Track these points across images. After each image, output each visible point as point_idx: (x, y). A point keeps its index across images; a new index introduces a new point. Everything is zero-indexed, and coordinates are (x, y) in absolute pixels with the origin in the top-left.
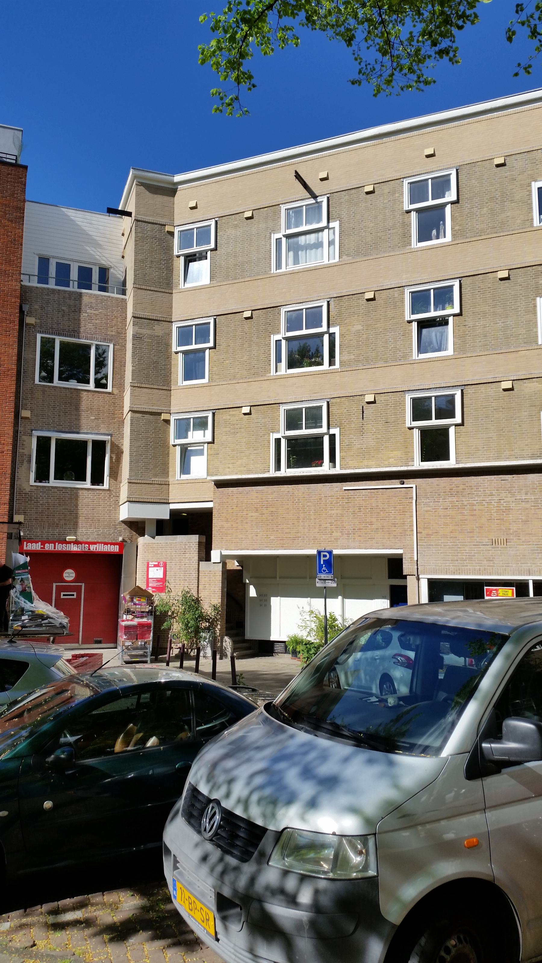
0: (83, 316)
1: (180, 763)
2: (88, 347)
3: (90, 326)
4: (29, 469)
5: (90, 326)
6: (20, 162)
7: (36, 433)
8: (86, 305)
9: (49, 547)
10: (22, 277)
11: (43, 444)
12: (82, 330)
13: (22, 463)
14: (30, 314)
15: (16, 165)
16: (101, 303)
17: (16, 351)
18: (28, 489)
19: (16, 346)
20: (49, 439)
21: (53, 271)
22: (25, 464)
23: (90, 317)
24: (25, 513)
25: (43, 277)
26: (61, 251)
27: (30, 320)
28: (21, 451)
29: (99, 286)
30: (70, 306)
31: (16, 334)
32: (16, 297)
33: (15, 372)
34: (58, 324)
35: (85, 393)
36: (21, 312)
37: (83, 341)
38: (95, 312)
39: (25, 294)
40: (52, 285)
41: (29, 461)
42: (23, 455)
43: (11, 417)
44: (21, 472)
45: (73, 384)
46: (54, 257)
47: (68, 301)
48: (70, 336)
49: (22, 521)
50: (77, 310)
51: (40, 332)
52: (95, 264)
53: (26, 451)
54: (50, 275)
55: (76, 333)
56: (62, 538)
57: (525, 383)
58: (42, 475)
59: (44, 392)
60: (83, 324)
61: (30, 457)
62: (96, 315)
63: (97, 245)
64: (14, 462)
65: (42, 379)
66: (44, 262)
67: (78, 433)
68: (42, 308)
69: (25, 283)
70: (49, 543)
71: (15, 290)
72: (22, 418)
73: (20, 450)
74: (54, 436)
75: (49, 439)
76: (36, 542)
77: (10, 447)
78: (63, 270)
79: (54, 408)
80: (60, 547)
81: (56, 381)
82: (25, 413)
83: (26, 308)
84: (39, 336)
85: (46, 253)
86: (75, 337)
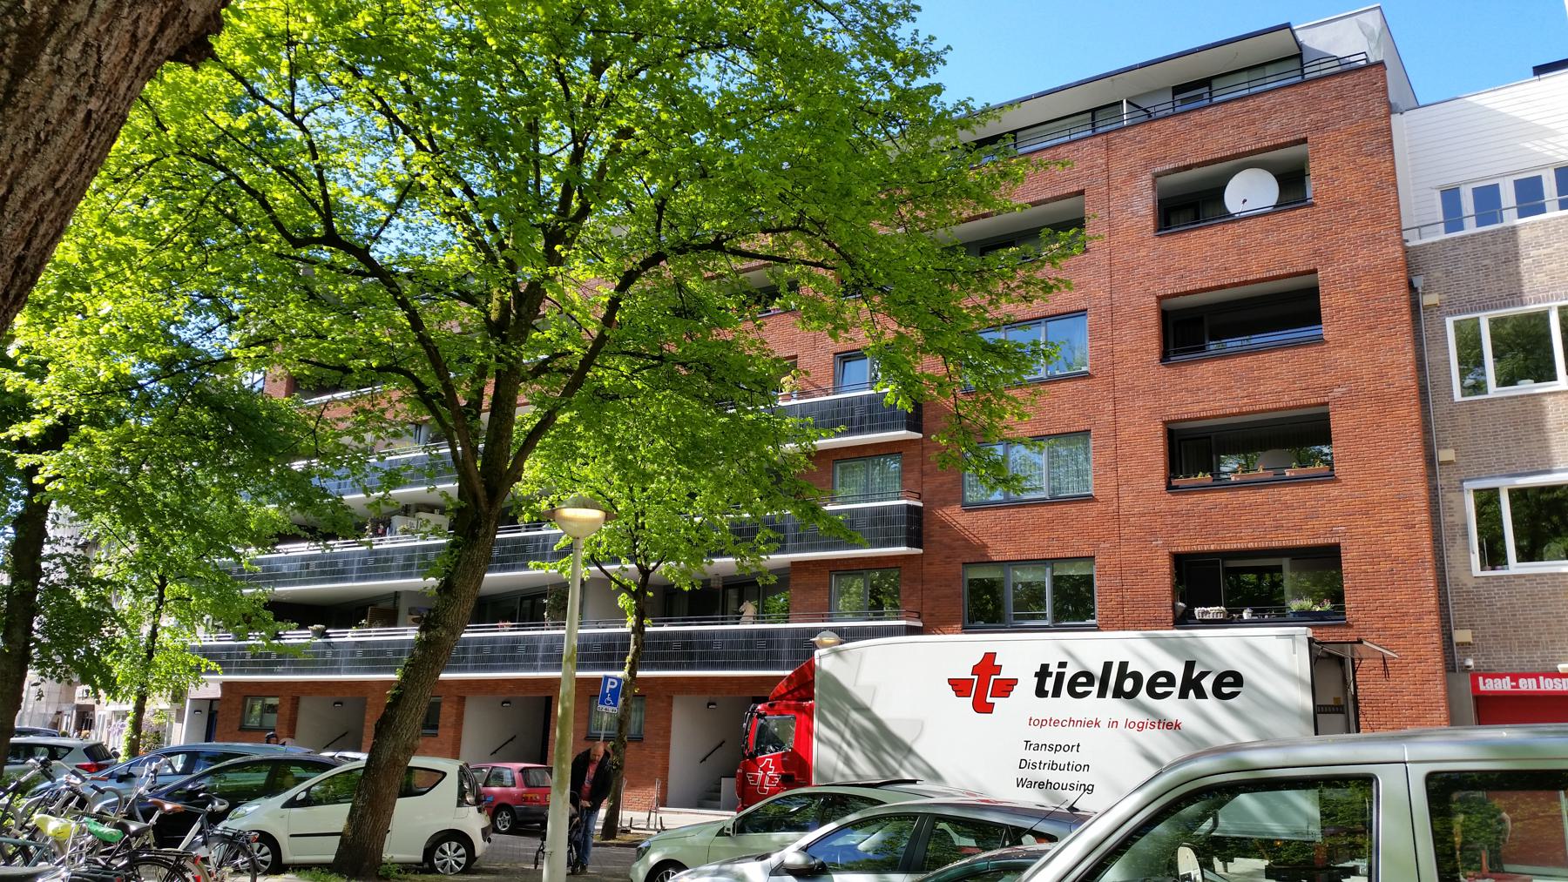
0: (1525, 264)
1: (178, 805)
2: (1543, 317)
3: (1541, 277)
4: (1467, 548)
5: (1541, 277)
6: (1372, 60)
7: (1470, 486)
8: (1527, 244)
9: (1527, 685)
10: (1406, 235)
11: (1487, 500)
12: (1526, 289)
13: (1454, 539)
14: (1428, 289)
15: (1369, 66)
16: (1556, 231)
17: (1410, 356)
18: (1471, 584)
19: (1409, 348)
20: (1495, 492)
21: (1468, 204)
22: (1459, 540)
23: (1538, 263)
24: (1472, 627)
25: (1453, 219)
26: (1472, 167)
27: (1428, 300)
28: (1448, 519)
29: (1561, 202)
30: (1496, 255)
31: (1406, 328)
32: (1400, 270)
33: (1414, 390)
34: (1480, 291)
35: (1549, 399)
36: (1412, 287)
37: (1532, 308)
38: (1543, 251)
39: (1412, 261)
40: (1471, 228)
41: (1466, 535)
42: (1453, 525)
43: (1419, 465)
44: (1453, 555)
45: (1527, 387)
46: (1504, 175)
47: (1491, 248)
48: (1505, 306)
49: (1470, 639)
50: (1512, 257)
51: (1451, 314)
52: (1545, 167)
53: (1457, 519)
54: (1465, 214)
55: (1516, 297)
56: (1549, 669)
57: (1212, 278)
58: (1493, 555)
59: (1472, 411)
60: (1525, 277)
61: (1465, 527)
62: (1549, 255)
63: (1543, 132)
64: (1437, 540)
65: (1466, 390)
66: (1450, 196)
67: (1549, 472)
68: (1447, 273)
69: (1414, 242)
70: (1527, 676)
71: (1395, 260)
72: (1441, 464)
73: (1446, 519)
74: (1504, 485)
75: (1495, 492)
76: (1502, 676)
77: (1425, 516)
78: (1487, 199)
79: (1495, 434)
80: (1548, 685)
81: (1493, 390)
82: (1445, 455)
83: (1419, 282)
84: (1450, 322)
85: (1449, 181)
86: (1514, 305)
